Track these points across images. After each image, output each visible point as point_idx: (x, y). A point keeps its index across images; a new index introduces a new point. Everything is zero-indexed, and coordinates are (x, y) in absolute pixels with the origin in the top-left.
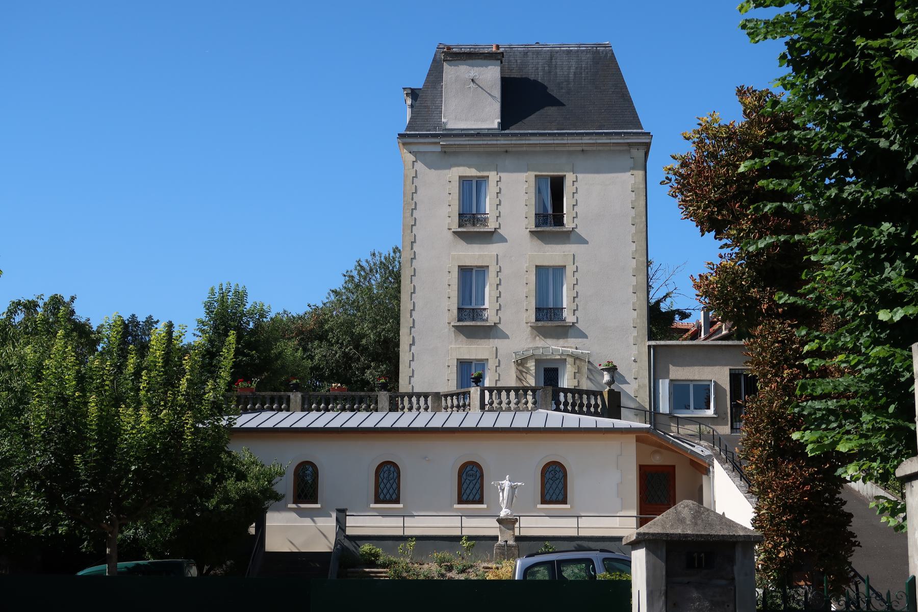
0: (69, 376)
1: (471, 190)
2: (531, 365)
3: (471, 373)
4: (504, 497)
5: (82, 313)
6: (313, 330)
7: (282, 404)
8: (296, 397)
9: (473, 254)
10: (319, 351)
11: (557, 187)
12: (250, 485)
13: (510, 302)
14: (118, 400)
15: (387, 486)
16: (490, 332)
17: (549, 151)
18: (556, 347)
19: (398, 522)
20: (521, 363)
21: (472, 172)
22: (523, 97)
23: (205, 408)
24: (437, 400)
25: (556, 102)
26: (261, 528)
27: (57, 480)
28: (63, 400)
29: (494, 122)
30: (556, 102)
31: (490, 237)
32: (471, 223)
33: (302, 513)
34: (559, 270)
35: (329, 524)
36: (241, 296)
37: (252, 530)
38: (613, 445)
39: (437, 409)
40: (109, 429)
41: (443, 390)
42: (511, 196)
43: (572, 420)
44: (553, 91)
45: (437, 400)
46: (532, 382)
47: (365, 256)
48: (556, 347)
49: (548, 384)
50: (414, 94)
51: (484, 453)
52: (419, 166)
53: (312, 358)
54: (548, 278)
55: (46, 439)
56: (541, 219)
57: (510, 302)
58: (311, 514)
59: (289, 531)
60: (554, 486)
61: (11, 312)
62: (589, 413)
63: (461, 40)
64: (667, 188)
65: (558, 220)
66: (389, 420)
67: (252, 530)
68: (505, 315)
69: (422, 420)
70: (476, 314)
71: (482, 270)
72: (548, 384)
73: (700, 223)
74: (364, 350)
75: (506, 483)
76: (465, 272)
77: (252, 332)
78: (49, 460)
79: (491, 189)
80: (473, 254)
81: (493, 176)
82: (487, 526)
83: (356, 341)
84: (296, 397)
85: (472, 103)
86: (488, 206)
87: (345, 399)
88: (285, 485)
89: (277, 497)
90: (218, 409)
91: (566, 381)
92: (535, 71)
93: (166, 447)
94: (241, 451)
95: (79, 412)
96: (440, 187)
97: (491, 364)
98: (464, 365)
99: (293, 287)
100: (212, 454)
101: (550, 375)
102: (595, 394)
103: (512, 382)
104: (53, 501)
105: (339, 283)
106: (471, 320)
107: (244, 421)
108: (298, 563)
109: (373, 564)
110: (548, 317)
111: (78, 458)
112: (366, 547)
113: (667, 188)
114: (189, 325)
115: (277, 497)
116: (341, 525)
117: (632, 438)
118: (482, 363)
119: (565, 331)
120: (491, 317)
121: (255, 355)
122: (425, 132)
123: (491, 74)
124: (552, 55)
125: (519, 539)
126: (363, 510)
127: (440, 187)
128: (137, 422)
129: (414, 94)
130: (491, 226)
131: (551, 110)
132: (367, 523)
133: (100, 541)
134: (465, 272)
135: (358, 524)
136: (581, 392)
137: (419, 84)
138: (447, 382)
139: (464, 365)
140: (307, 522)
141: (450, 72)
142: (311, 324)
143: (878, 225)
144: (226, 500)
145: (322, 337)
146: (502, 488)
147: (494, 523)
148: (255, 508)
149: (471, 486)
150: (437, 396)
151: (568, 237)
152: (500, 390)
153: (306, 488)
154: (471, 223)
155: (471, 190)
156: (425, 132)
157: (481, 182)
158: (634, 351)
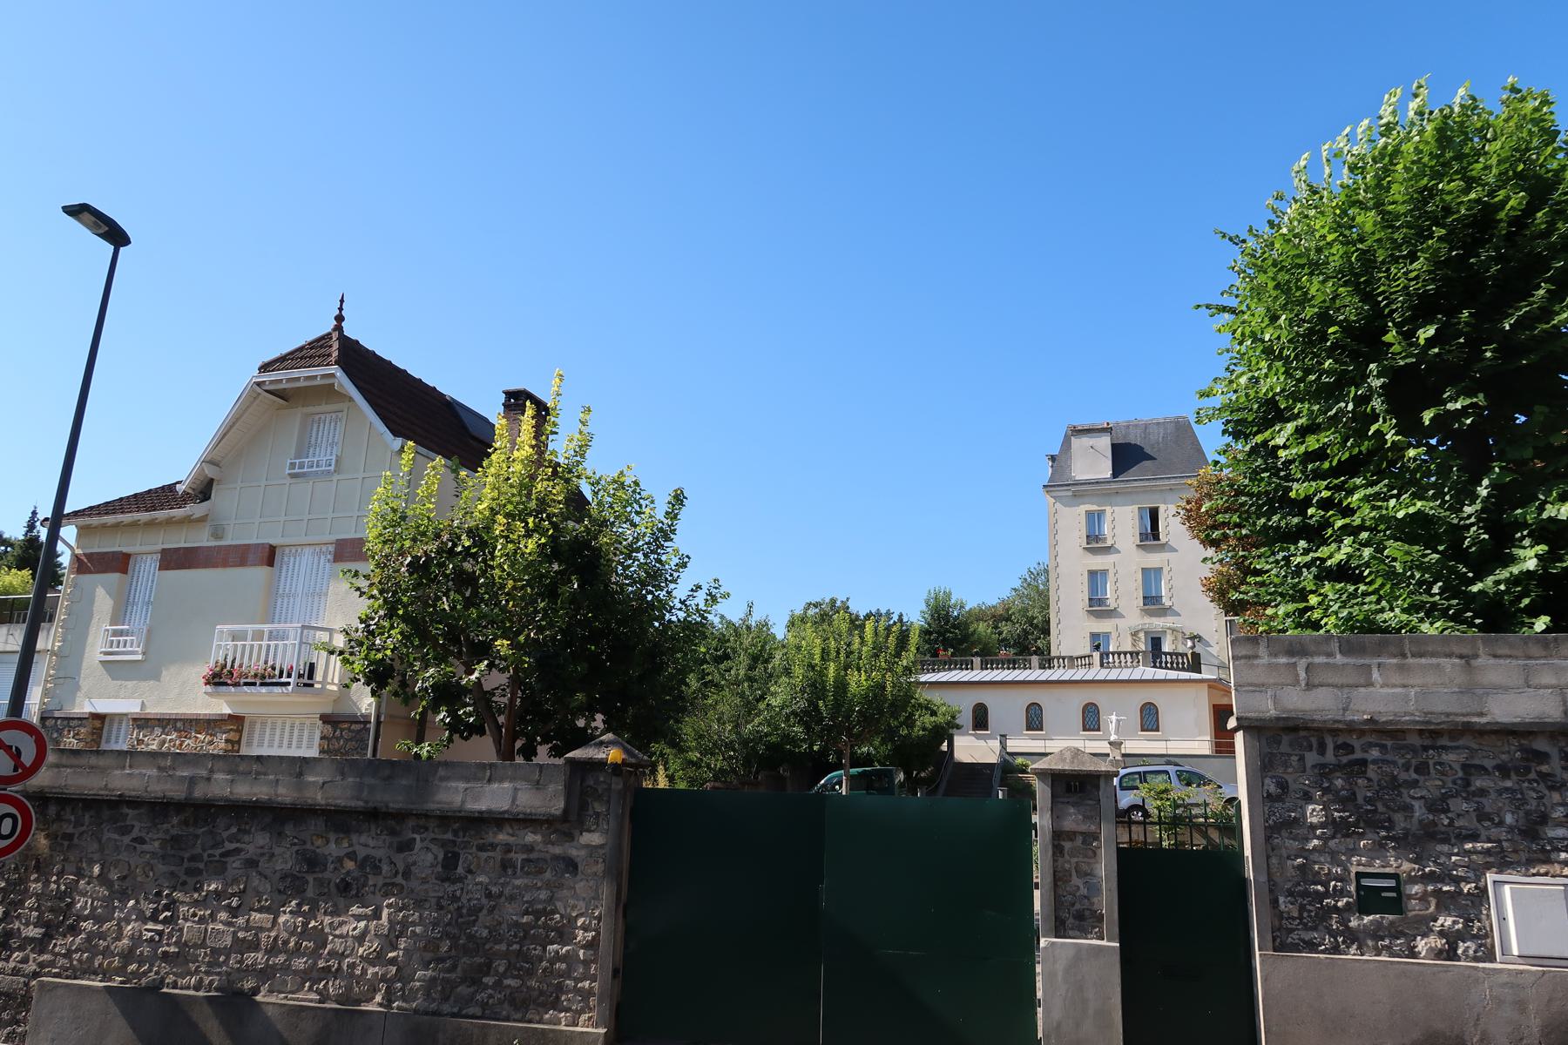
0: (817, 651)
1: (1094, 519)
2: (1142, 635)
3: (1097, 642)
4: (1112, 727)
5: (853, 608)
6: (1000, 617)
7: (968, 666)
8: (977, 660)
9: (1098, 562)
10: (1006, 628)
11: (1154, 515)
12: (940, 719)
13: (1125, 592)
14: (846, 668)
15: (1034, 719)
16: (1112, 613)
17: (1145, 490)
18: (1158, 623)
19: (1041, 743)
20: (1135, 634)
21: (1095, 508)
22: (1126, 456)
23: (899, 670)
24: (1072, 661)
25: (1150, 458)
26: (951, 745)
27: (809, 717)
28: (812, 667)
29: (1108, 474)
30: (1150, 458)
31: (1108, 550)
32: (1095, 542)
33: (978, 737)
34: (1159, 570)
35: (995, 744)
36: (948, 595)
37: (944, 747)
38: (1191, 690)
39: (1072, 667)
40: (841, 685)
41: (1075, 654)
42: (1123, 522)
43: (1173, 675)
44: (1148, 450)
45: (1072, 661)
46: (1142, 647)
47: (1033, 566)
48: (1158, 623)
49: (1156, 652)
50: (1053, 458)
51: (1099, 697)
52: (1058, 505)
53: (1000, 633)
54: (1150, 576)
55: (803, 691)
56: (1143, 536)
57: (1125, 592)
58: (985, 738)
59: (970, 749)
60: (1150, 719)
61: (806, 609)
62: (1172, 668)
63: (1083, 422)
64: (1178, 519)
65: (1156, 537)
66: (1045, 675)
67: (944, 747)
68: (1122, 602)
69: (1068, 675)
70: (1101, 602)
71: (1104, 572)
72: (1156, 652)
73: (1202, 542)
74: (1036, 627)
75: (1114, 718)
76: (1093, 574)
77: (957, 618)
78: (803, 704)
79: (1108, 517)
80: (1098, 562)
81: (1108, 509)
82: (1103, 747)
83: (1030, 621)
84: (1035, 659)
85: (1093, 462)
86: (1106, 529)
87: (1009, 662)
88: (966, 718)
89: (958, 727)
90: (908, 670)
91: (1166, 647)
92: (1135, 438)
93: (875, 696)
94: (923, 695)
95: (822, 674)
96: (1073, 519)
97: (1114, 635)
98: (1094, 636)
99: (981, 590)
100: (905, 702)
101: (1156, 643)
102: (1183, 655)
103: (1129, 648)
104: (808, 729)
105: (1017, 584)
106: (1098, 606)
107: (923, 678)
108: (977, 771)
109: (1024, 772)
110: (1151, 601)
111: (821, 703)
112: (1020, 760)
113: (1178, 519)
114: (916, 616)
115: (958, 727)
116: (1003, 746)
117: (1204, 688)
118: (1107, 635)
119: (1165, 612)
120: (1112, 603)
121: (950, 636)
122: (1061, 484)
123: (1104, 442)
124: (1146, 426)
125: (1124, 755)
126: (1019, 735)
127: (1073, 519)
128: (858, 682)
129: (1053, 458)
130: (1109, 543)
131: (1147, 463)
132: (1021, 743)
133: (840, 754)
134: (1093, 574)
135: (1014, 745)
136: (1177, 655)
137: (1056, 452)
138: (1084, 648)
139: (1094, 636)
140: (982, 743)
141: (1076, 442)
142: (1000, 611)
143: (1296, 543)
144: (924, 729)
145: (1008, 619)
146: (1111, 721)
147: (1106, 744)
148: (944, 732)
149: (1091, 719)
150: (1071, 658)
151: (1164, 547)
152: (1119, 654)
153: (981, 720)
154: (1095, 542)
155: (1094, 519)
156: (1061, 484)
157: (1101, 514)
158: (1215, 624)
